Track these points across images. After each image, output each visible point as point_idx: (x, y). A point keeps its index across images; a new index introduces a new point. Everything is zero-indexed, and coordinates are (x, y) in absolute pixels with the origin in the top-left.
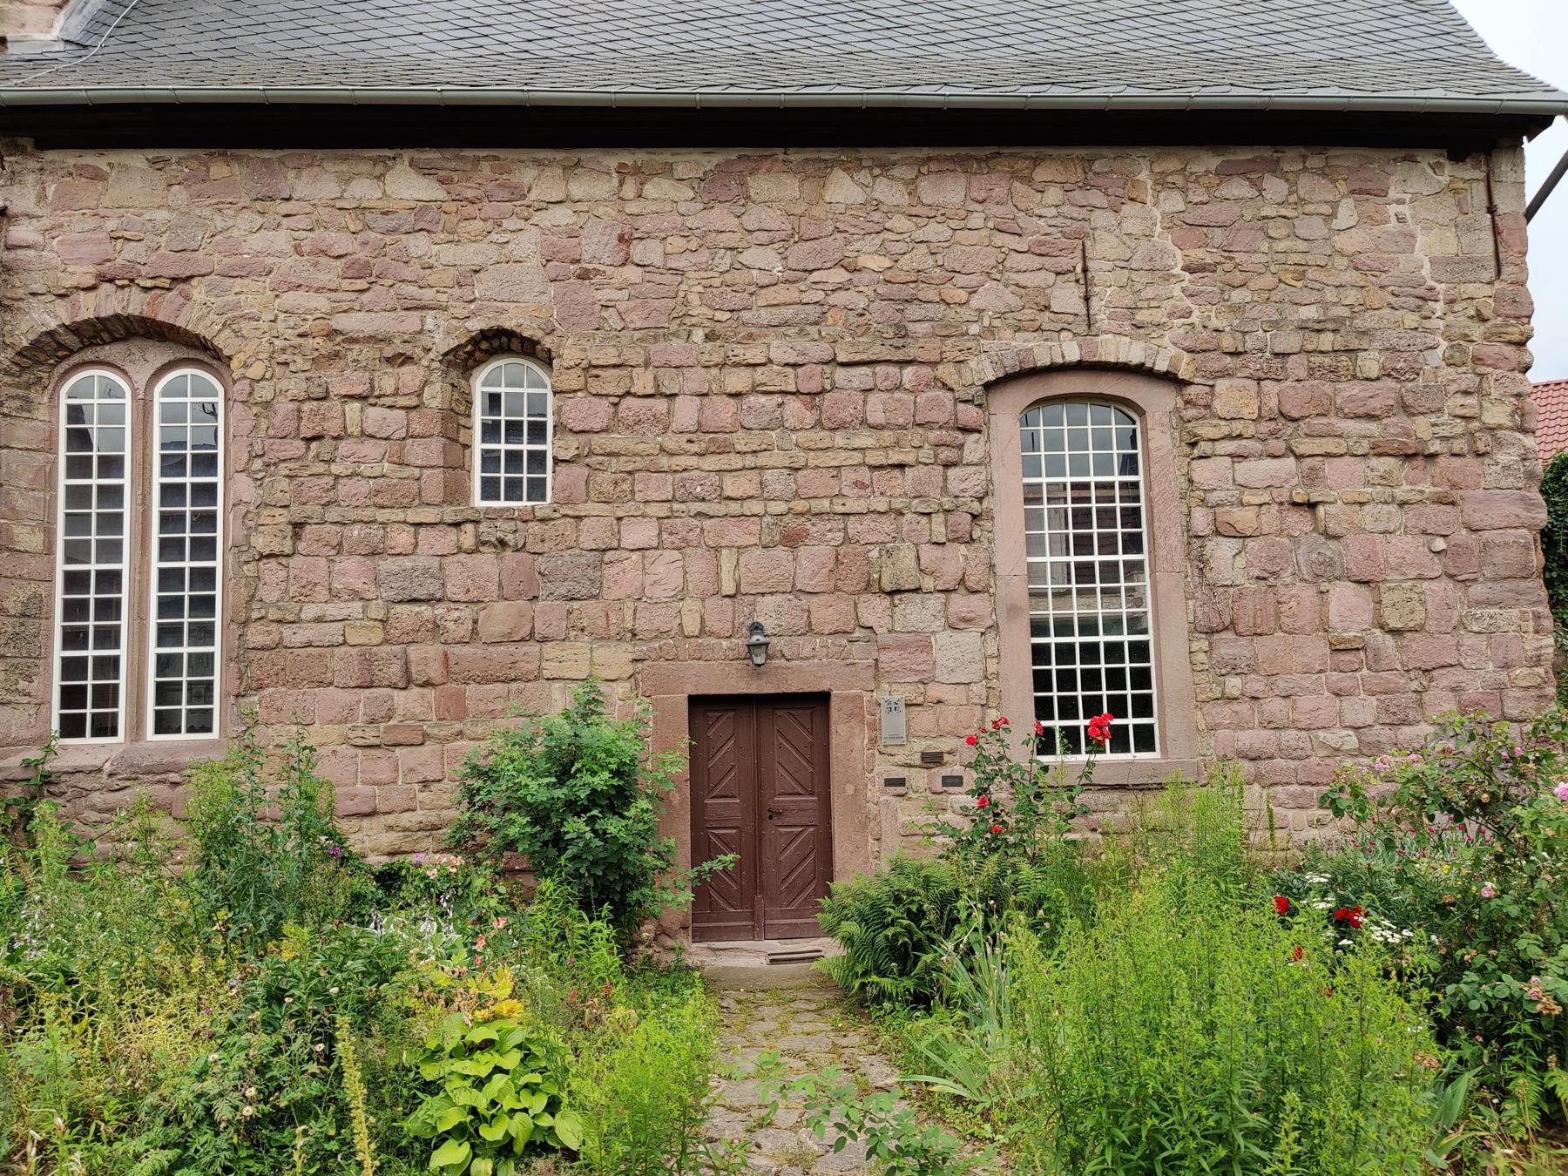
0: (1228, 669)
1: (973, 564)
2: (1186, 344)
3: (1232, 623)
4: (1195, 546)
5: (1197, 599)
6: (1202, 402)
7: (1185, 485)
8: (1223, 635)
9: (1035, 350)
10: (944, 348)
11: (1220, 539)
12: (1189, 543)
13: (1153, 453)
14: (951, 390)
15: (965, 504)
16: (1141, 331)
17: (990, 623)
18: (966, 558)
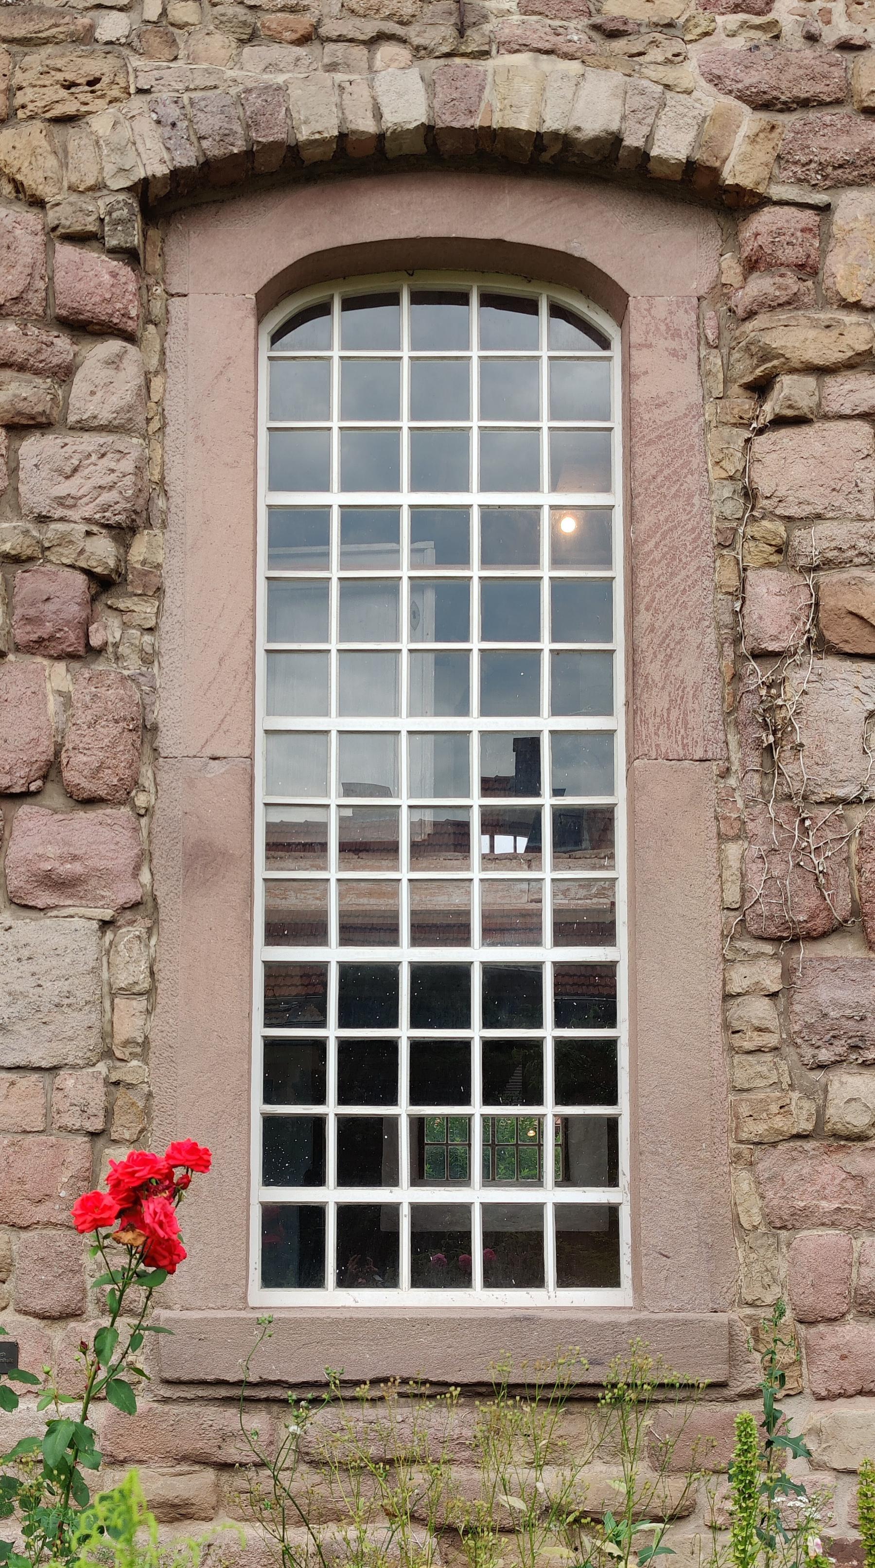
0: (840, 1047)
1: (83, 717)
2: (751, 79)
3: (857, 911)
4: (752, 682)
5: (751, 839)
6: (790, 254)
7: (734, 508)
8: (829, 949)
9: (295, 92)
10: (19, 78)
11: (830, 663)
12: (737, 677)
13: (645, 415)
14: (38, 203)
15: (65, 540)
16: (619, 45)
17: (129, 893)
18: (67, 700)
